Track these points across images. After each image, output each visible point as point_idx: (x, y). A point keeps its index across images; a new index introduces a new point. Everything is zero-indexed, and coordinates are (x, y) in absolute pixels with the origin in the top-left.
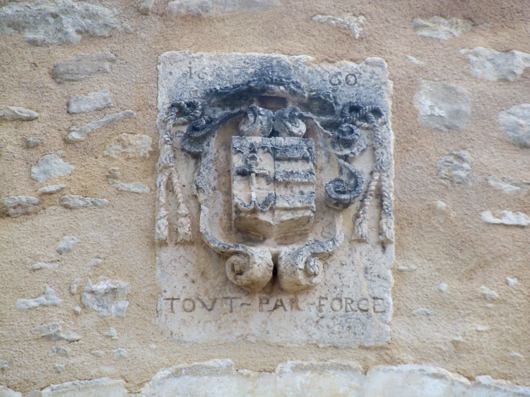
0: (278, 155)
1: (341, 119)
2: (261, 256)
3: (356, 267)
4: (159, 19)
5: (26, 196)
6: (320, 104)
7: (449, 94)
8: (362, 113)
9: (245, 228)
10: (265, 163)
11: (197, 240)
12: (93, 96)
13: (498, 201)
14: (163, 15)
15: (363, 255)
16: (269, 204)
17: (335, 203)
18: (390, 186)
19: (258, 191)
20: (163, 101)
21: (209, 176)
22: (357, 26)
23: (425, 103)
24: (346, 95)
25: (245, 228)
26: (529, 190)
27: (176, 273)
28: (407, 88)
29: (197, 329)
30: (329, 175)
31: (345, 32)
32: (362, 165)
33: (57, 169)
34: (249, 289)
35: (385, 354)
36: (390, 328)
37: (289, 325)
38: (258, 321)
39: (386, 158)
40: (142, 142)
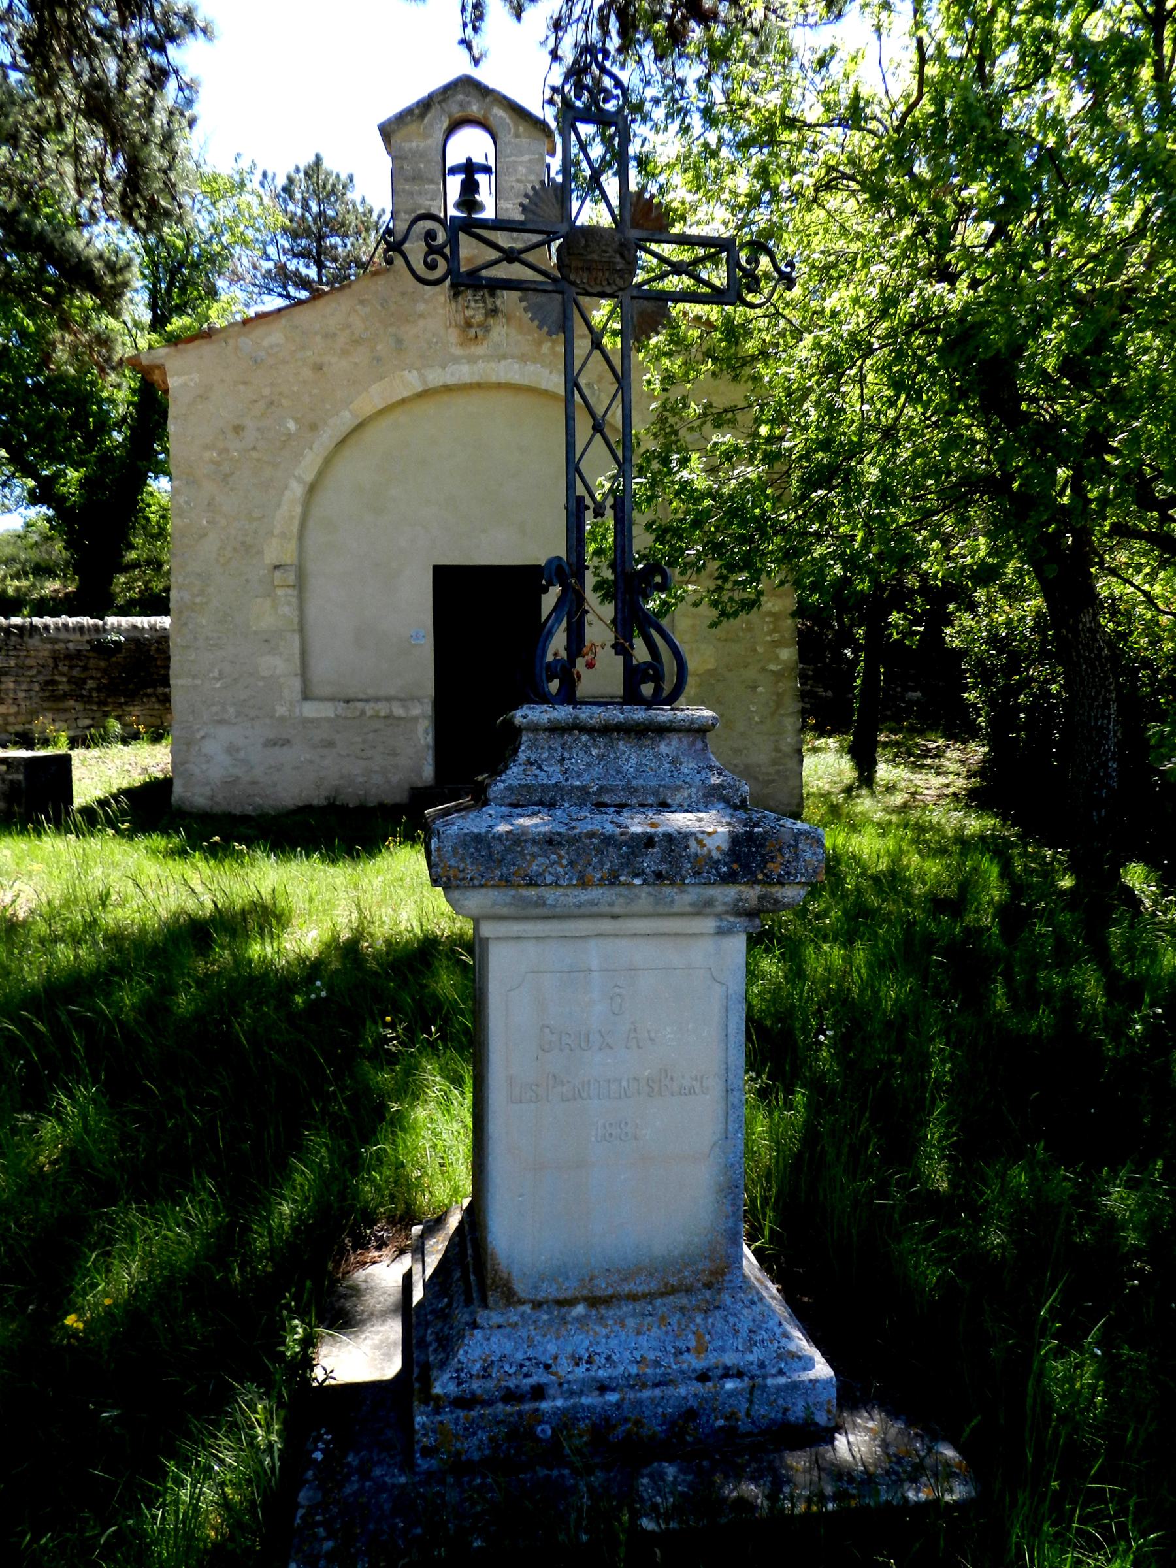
10: (473, 304)
35: (504, 357)
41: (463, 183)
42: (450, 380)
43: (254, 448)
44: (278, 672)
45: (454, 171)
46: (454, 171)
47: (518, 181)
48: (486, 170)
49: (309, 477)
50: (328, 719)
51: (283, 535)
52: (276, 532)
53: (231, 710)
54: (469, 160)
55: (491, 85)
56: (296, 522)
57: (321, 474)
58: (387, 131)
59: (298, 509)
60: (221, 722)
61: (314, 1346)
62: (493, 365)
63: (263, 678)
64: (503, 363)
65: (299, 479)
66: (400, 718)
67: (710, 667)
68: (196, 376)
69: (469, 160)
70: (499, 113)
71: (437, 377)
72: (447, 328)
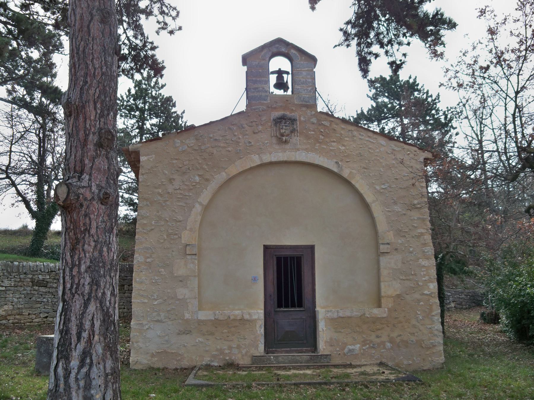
0: (286, 126)
1: (293, 121)
2: (284, 138)
3: (295, 139)
4: (528, 352)
5: (257, 131)
6: (290, 119)
7: (305, 117)
8: (295, 120)
9: (282, 135)
10: (284, 127)
11: (277, 136)
12: (264, 118)
13: (311, 131)
14: (271, 108)
15: (295, 138)
16: (285, 132)
17: (292, 132)
18: (298, 129)
19: (283, 131)
20: (272, 119)
21: (278, 128)
22: (294, 109)
23: (302, 119)
24: (293, 118)
25: (282, 135)
26: (533, 390)
27: (274, 140)
28: (300, 117)
29: (277, 147)
30: (292, 128)
31: (293, 109)
32: (295, 127)
33: (260, 127)
34: (283, 142)
35: (298, 150)
36: (299, 146)
37: (287, 146)
38: (284, 146)
39: (298, 126)
40: (270, 124)
41: (277, 77)
42: (274, 159)
43: (179, 189)
44: (186, 297)
45: (273, 73)
46: (273, 73)
47: (303, 78)
48: (287, 73)
49: (205, 203)
50: (211, 320)
51: (191, 230)
52: (188, 228)
53: (162, 314)
54: (280, 69)
55: (290, 42)
56: (198, 223)
57: (211, 201)
58: (246, 59)
59: (199, 218)
60: (158, 321)
61: (358, 16)
62: (293, 153)
63: (179, 299)
64: (298, 153)
65: (200, 204)
66: (248, 320)
67: (398, 293)
68: (154, 156)
69: (280, 69)
70: (293, 51)
71: (267, 158)
72: (272, 137)
